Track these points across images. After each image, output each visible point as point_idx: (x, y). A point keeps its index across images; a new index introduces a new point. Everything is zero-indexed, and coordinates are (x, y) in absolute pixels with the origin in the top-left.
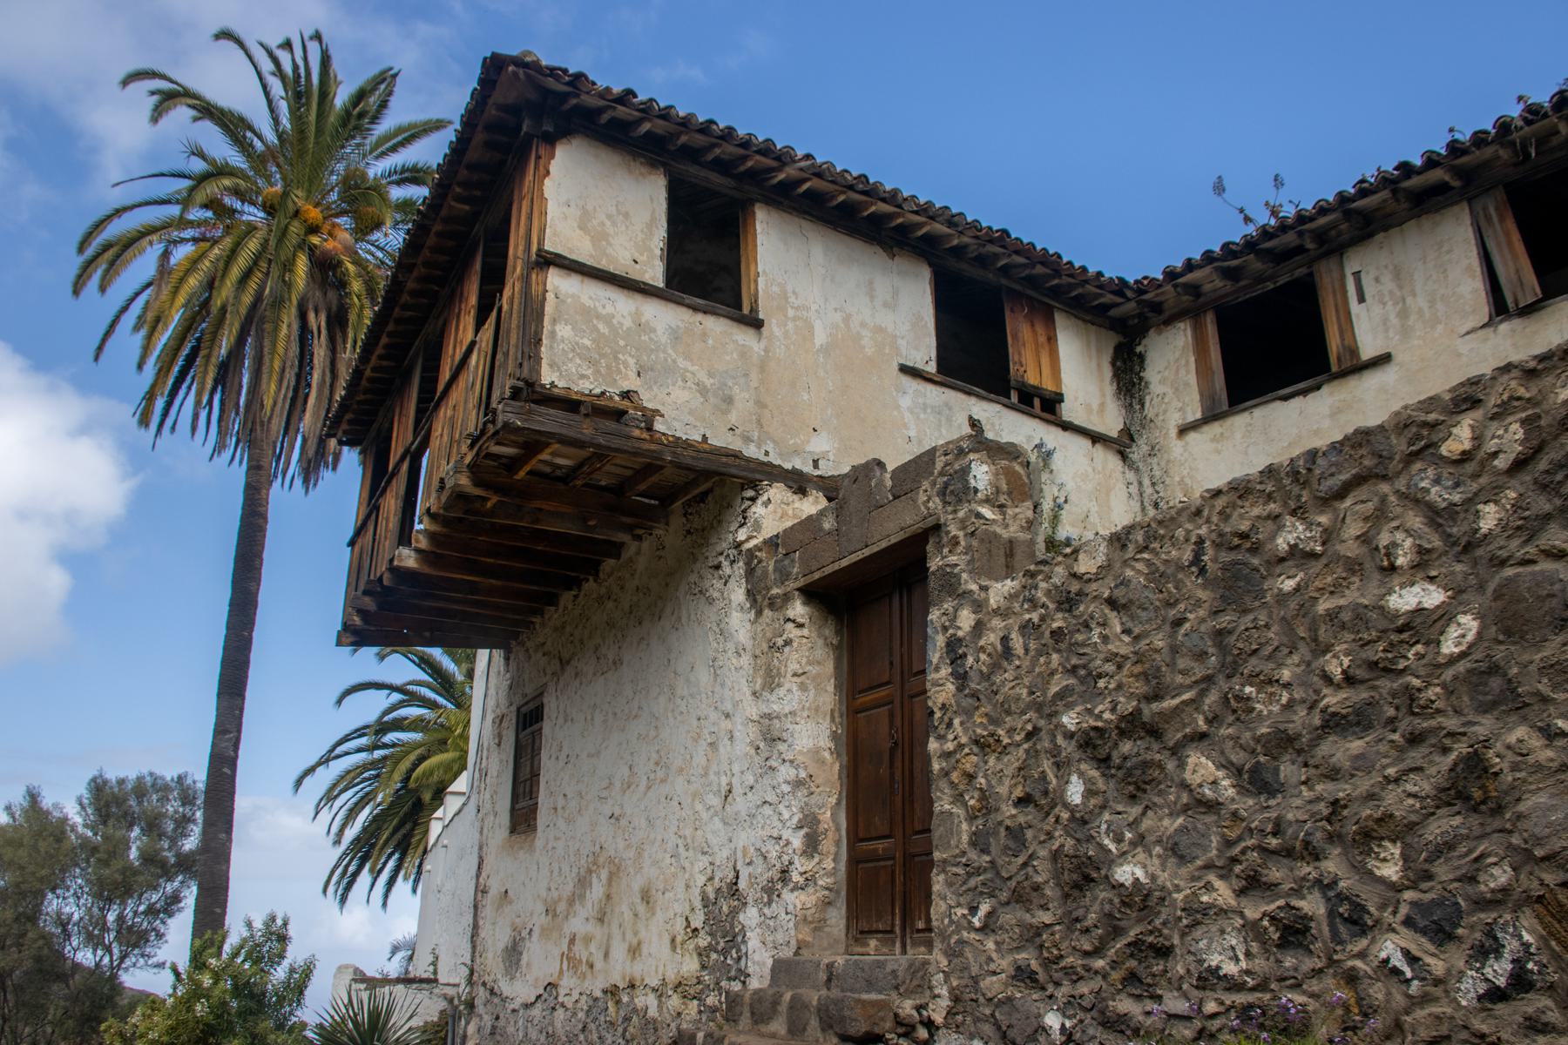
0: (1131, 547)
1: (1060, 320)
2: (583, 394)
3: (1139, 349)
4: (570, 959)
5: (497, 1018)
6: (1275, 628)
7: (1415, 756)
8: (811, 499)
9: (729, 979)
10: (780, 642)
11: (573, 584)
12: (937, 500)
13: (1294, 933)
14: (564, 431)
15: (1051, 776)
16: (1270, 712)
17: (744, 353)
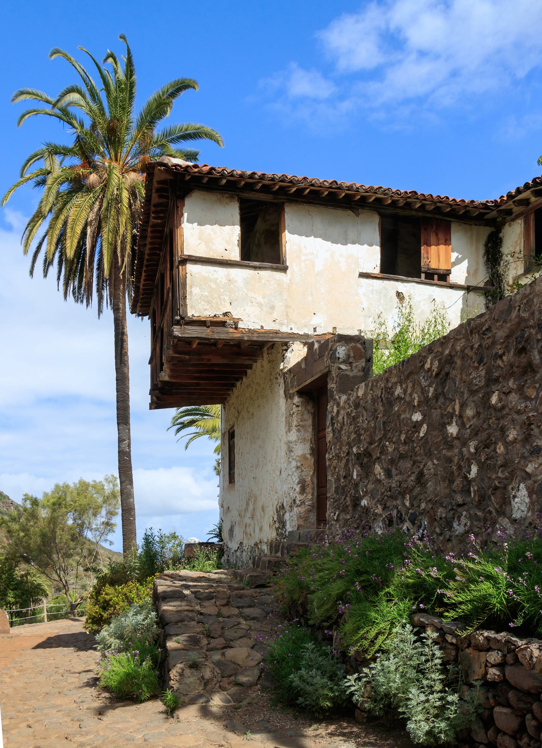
1: (454, 227)
12: (329, 360)
14: (199, 336)
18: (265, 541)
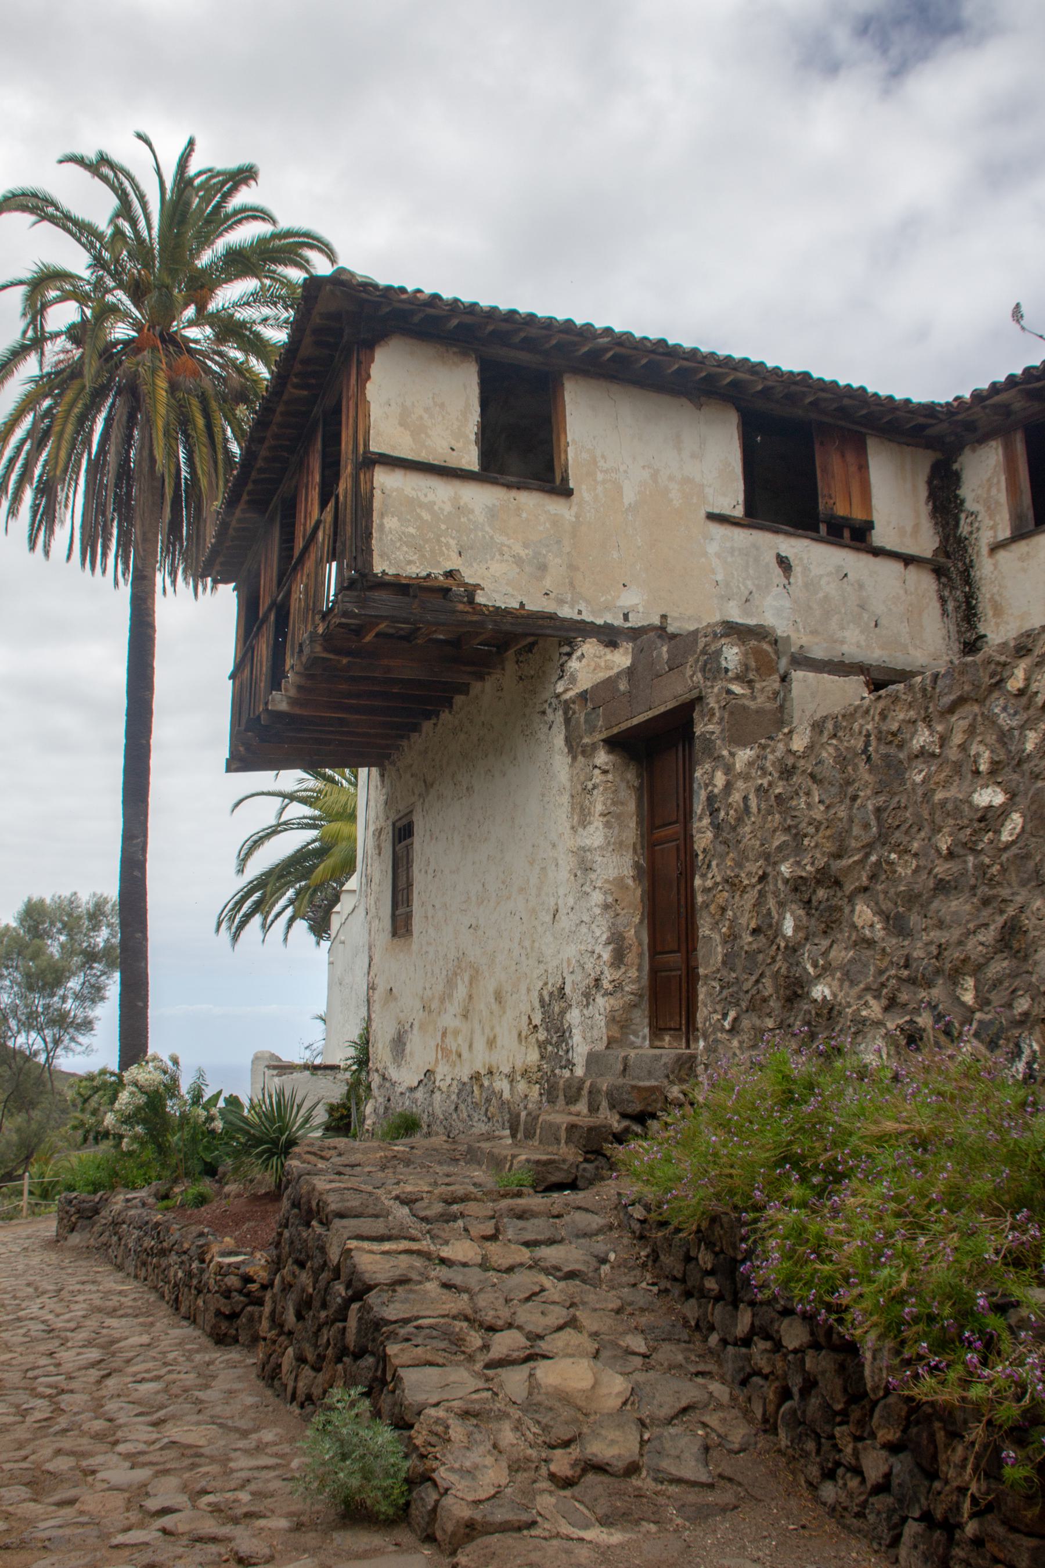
0: (826, 734)
2: (410, 578)
3: (956, 466)
4: (443, 1050)
8: (621, 650)
9: (561, 1067)
10: (590, 786)
12: (699, 675)
13: (913, 1038)
15: (774, 914)
18: (506, 1070)
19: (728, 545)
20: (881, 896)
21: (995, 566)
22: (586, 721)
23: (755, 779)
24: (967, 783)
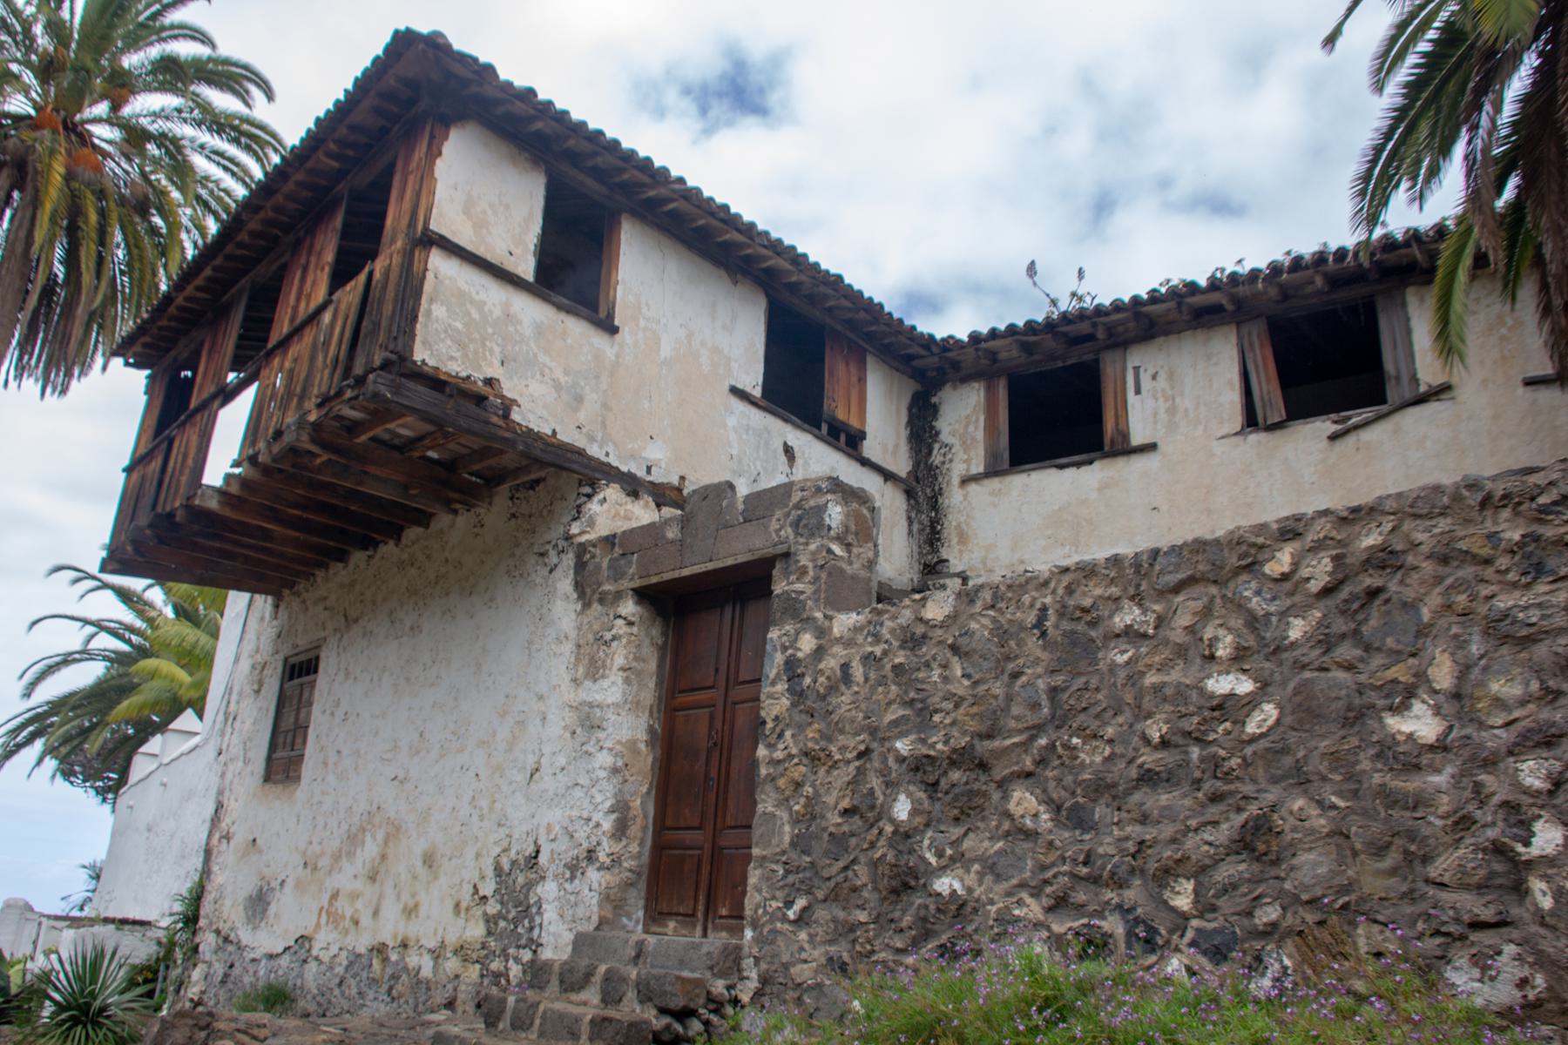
2: (450, 375)
3: (934, 400)
4: (331, 915)
5: (231, 966)
6: (1104, 692)
7: (1213, 811)
9: (518, 947)
10: (608, 636)
11: (368, 543)
12: (789, 530)
13: (1095, 945)
15: (878, 793)
16: (1092, 762)
17: (598, 356)
19: (745, 422)
20: (1052, 784)
21: (965, 497)
22: (609, 567)
23: (861, 646)
24: (1195, 668)
